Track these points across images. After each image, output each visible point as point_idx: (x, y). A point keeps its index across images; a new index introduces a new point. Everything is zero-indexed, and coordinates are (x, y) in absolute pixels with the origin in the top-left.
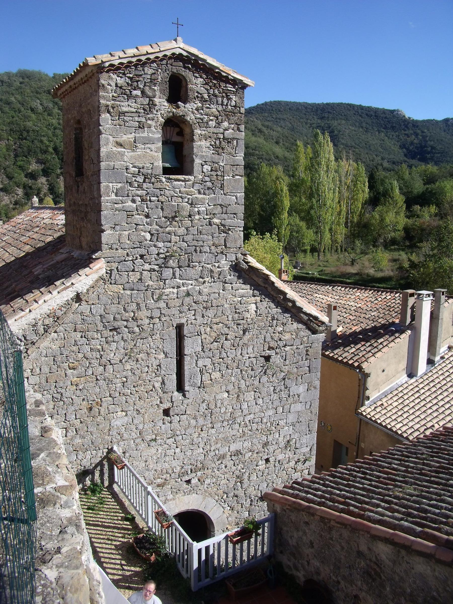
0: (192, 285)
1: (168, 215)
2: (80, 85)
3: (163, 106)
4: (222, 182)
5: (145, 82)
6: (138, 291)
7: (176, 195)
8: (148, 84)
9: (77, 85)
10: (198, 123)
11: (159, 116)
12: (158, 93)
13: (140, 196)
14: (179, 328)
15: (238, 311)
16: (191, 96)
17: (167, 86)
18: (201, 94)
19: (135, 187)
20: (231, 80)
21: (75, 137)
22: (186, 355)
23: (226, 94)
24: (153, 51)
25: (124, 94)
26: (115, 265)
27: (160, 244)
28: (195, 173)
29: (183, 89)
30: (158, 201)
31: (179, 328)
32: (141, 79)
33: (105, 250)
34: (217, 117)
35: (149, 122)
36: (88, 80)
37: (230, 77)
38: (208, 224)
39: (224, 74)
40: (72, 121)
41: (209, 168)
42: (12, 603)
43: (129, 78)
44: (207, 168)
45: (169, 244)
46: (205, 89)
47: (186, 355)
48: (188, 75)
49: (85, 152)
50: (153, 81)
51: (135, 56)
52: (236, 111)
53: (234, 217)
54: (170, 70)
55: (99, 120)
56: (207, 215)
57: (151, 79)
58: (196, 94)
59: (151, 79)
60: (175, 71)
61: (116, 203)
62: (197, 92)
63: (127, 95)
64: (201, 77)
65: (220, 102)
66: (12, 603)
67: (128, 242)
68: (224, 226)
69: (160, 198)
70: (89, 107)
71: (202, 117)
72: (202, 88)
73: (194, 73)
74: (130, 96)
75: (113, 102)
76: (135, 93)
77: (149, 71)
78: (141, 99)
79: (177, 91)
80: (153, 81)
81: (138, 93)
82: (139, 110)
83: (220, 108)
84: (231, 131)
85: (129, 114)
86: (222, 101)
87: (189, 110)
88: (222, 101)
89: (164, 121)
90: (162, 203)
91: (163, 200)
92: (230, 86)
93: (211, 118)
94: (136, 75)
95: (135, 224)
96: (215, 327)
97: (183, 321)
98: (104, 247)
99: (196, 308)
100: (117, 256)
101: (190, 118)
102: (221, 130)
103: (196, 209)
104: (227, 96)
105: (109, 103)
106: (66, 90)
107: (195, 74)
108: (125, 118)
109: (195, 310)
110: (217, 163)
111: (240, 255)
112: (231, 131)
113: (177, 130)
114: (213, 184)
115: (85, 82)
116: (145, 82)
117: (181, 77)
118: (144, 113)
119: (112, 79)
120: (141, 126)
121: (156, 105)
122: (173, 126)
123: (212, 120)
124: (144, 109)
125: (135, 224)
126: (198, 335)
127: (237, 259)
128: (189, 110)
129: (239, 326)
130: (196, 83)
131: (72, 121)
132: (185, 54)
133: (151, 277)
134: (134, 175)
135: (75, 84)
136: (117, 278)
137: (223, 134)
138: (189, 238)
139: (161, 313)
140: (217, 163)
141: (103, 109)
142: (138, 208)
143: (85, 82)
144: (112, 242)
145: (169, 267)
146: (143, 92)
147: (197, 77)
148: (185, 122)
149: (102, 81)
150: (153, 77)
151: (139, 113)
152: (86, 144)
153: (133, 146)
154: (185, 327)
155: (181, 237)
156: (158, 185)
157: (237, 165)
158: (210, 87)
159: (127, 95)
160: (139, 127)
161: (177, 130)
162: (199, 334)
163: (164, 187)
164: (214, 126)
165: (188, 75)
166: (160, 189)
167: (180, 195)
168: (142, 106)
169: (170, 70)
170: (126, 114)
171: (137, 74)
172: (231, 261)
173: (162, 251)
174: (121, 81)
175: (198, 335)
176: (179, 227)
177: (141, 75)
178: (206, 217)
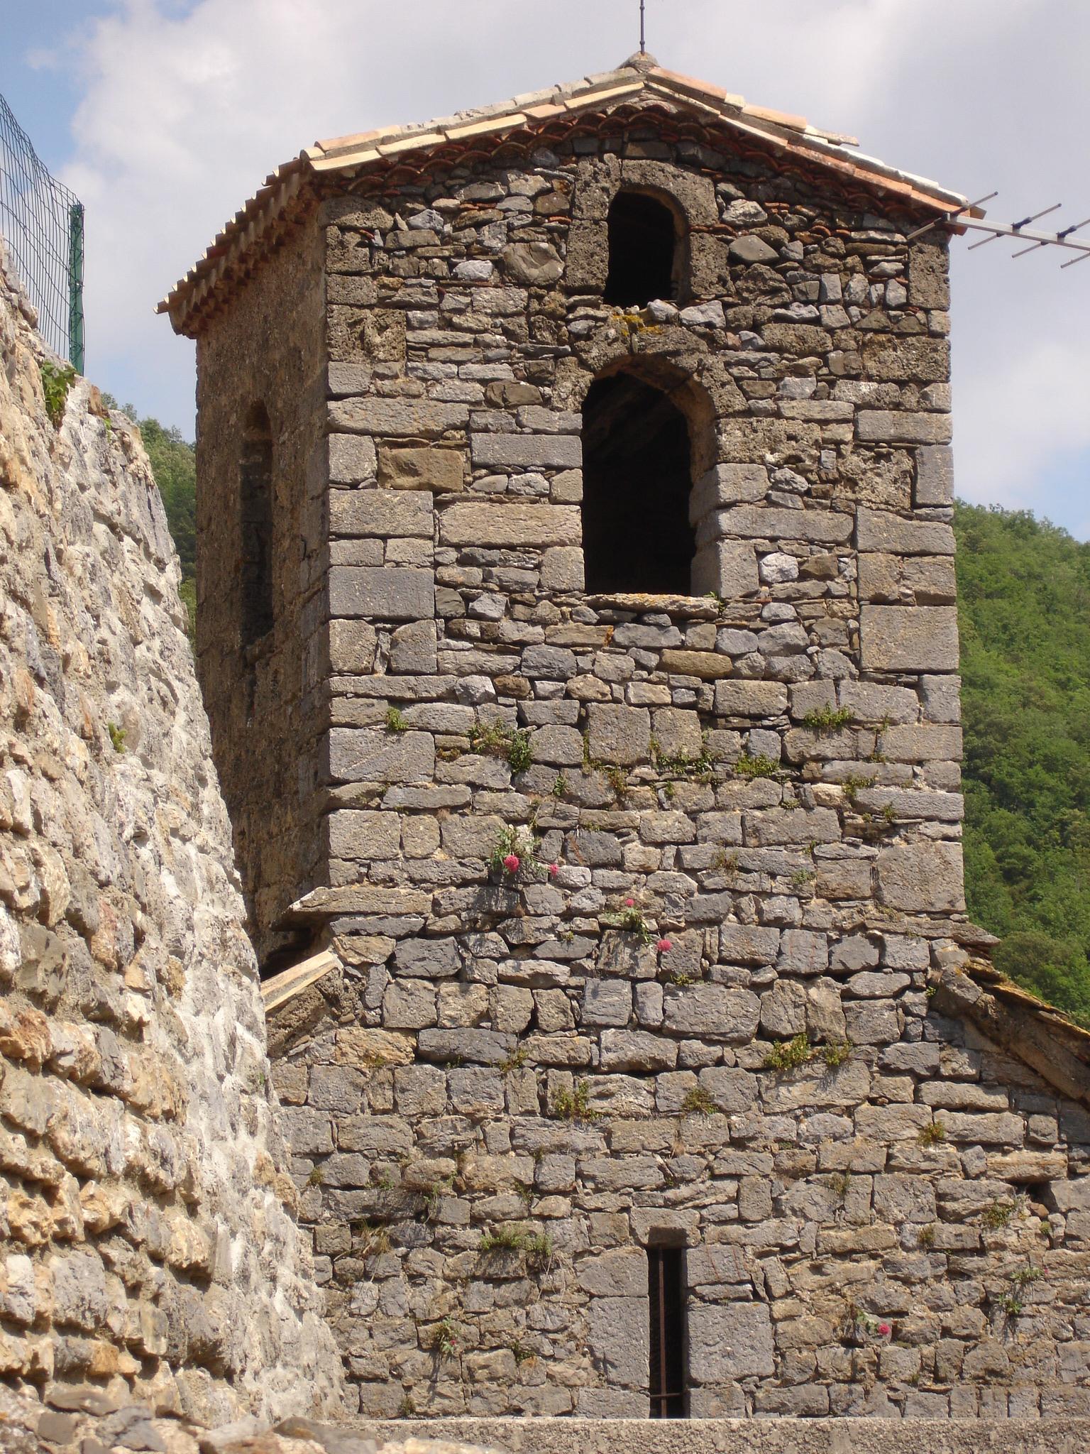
1: (609, 755)
2: (264, 258)
5: (510, 228)
8: (520, 234)
9: (251, 265)
10: (738, 380)
14: (667, 1255)
15: (950, 1206)
17: (603, 238)
21: (246, 483)
22: (697, 1384)
23: (863, 256)
25: (428, 276)
27: (578, 874)
29: (680, 248)
31: (667, 1255)
32: (490, 213)
34: (823, 356)
36: (289, 233)
40: (233, 419)
41: (790, 563)
42: (9, 1377)
45: (611, 877)
46: (767, 240)
47: (697, 1384)
48: (695, 192)
49: (282, 524)
52: (908, 324)
53: (915, 775)
55: (326, 378)
57: (534, 213)
59: (534, 213)
60: (636, 178)
63: (437, 278)
66: (9, 1377)
67: (439, 855)
68: (859, 808)
69: (576, 683)
70: (294, 339)
73: (716, 182)
78: (492, 291)
81: (480, 267)
82: (487, 337)
88: (846, 288)
90: (584, 701)
91: (590, 693)
95: (471, 784)
96: (837, 1268)
97: (682, 1220)
98: (340, 869)
99: (743, 1167)
102: (845, 408)
104: (868, 265)
106: (211, 293)
108: (430, 367)
109: (737, 1177)
111: (951, 947)
114: (809, 630)
115: (280, 243)
116: (510, 228)
117: (663, 200)
118: (510, 347)
124: (506, 332)
125: (471, 784)
126: (757, 1296)
127: (935, 963)
129: (963, 1285)
131: (233, 419)
132: (671, 108)
135: (243, 259)
136: (388, 1004)
137: (855, 422)
139: (579, 1175)
141: (340, 332)
143: (280, 243)
144: (372, 852)
146: (501, 265)
151: (488, 346)
152: (282, 491)
154: (692, 1255)
155: (671, 851)
162: (763, 1293)
165: (695, 192)
168: (499, 320)
170: (433, 353)
172: (910, 972)
173: (579, 901)
175: (757, 1296)
177: (498, 199)
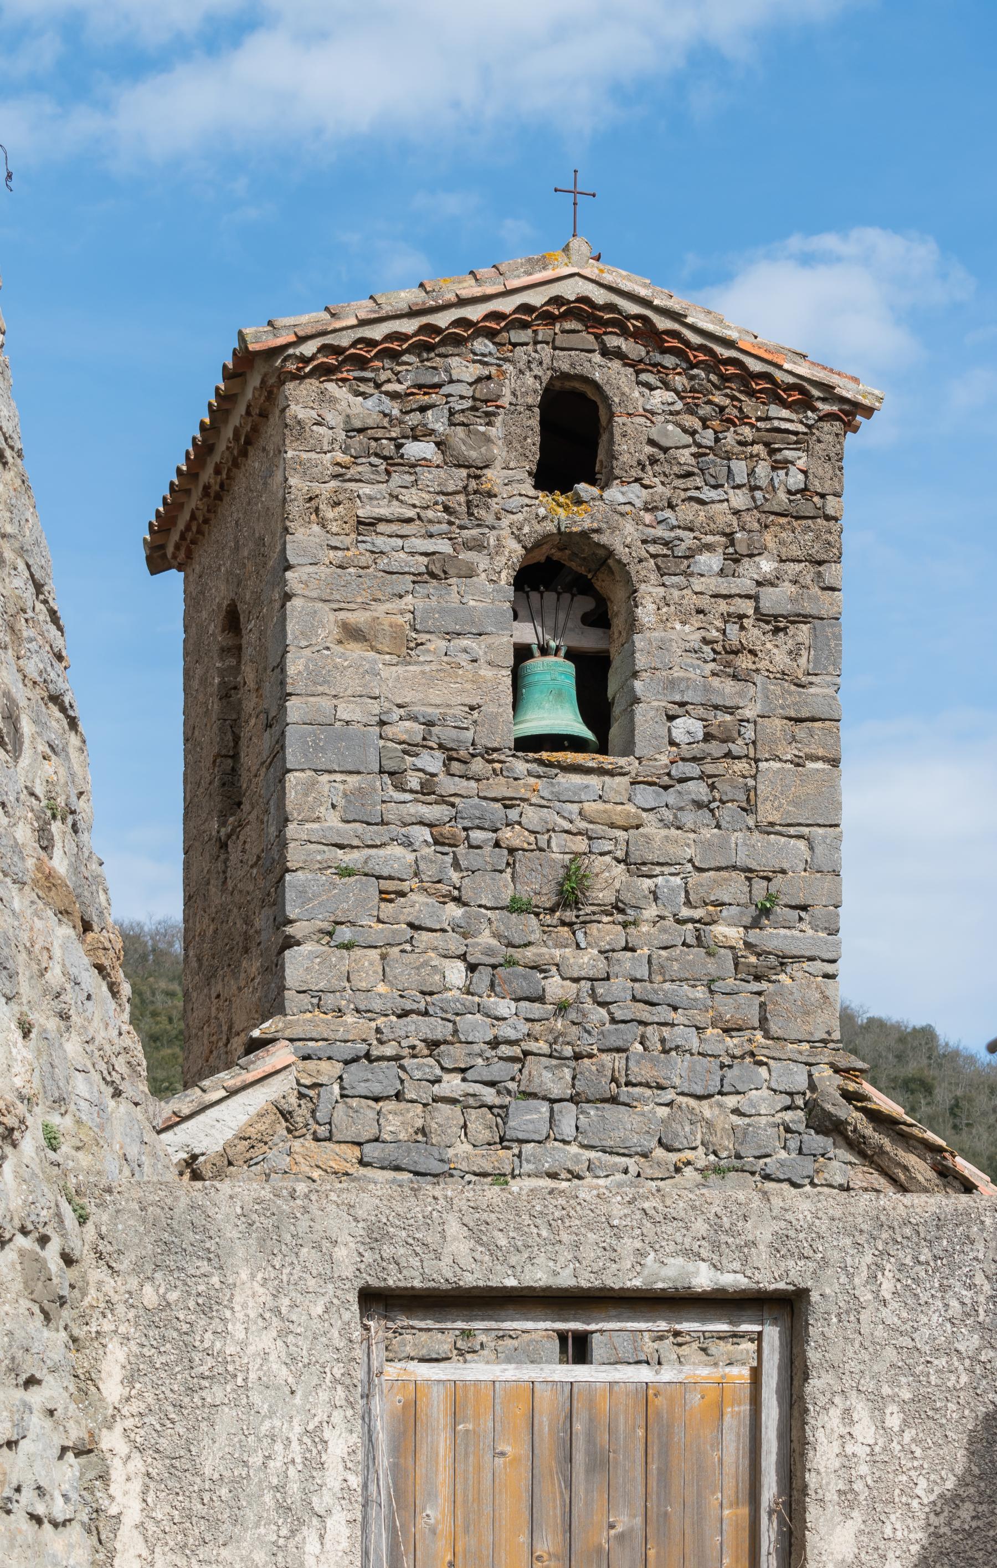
0: (626, 1172)
3: (524, 512)
4: (751, 782)
6: (417, 1173)
7: (567, 825)
10: (654, 556)
11: (506, 532)
12: (498, 451)
13: (430, 826)
16: (625, 458)
18: (665, 450)
19: (411, 791)
20: (790, 388)
24: (477, 291)
26: (328, 1070)
28: (641, 748)
30: (497, 845)
33: (299, 1018)
34: (730, 536)
35: (465, 556)
37: (779, 376)
38: (691, 940)
39: (755, 366)
41: (698, 728)
43: (394, 396)
44: (687, 728)
50: (484, 406)
51: (412, 313)
53: (801, 919)
54: (547, 361)
56: (688, 903)
58: (649, 450)
61: (341, 847)
62: (651, 442)
64: (667, 386)
65: (741, 478)
67: (382, 988)
71: (668, 535)
72: (670, 427)
74: (394, 462)
75: (334, 484)
76: (414, 449)
77: (463, 369)
79: (572, 440)
80: (484, 406)
83: (739, 499)
84: (787, 588)
85: (394, 528)
86: (751, 473)
87: (615, 513)
88: (751, 473)
89: (522, 552)
91: (516, 843)
92: (785, 413)
93: (709, 539)
94: (420, 387)
95: (411, 925)
100: (339, 1035)
101: (625, 539)
103: (647, 883)
105: (317, 488)
107: (644, 377)
110: (730, 710)
112: (787, 588)
113: (585, 604)
114: (712, 787)
118: (450, 523)
119: (333, 400)
120: (436, 572)
121: (491, 495)
122: (568, 589)
123: (709, 547)
127: (812, 1087)
128: (615, 513)
130: (643, 409)
132: (600, 296)
133: (465, 1126)
134: (410, 748)
137: (756, 598)
138: (618, 988)
140: (730, 710)
142: (422, 866)
145: (534, 1095)
147: (651, 388)
148: (604, 559)
149: (297, 410)
150: (483, 390)
153: (408, 646)
156: (499, 788)
157: (813, 720)
158: (704, 420)
159: (385, 458)
160: (433, 575)
161: (585, 604)
163: (523, 793)
164: (716, 568)
165: (614, 378)
166: (508, 803)
167: (584, 825)
168: (441, 498)
169: (547, 361)
170: (381, 527)
171: (422, 380)
172: (791, 1094)
174: (367, 409)
176: (578, 946)
177: (439, 386)
178: (685, 912)
